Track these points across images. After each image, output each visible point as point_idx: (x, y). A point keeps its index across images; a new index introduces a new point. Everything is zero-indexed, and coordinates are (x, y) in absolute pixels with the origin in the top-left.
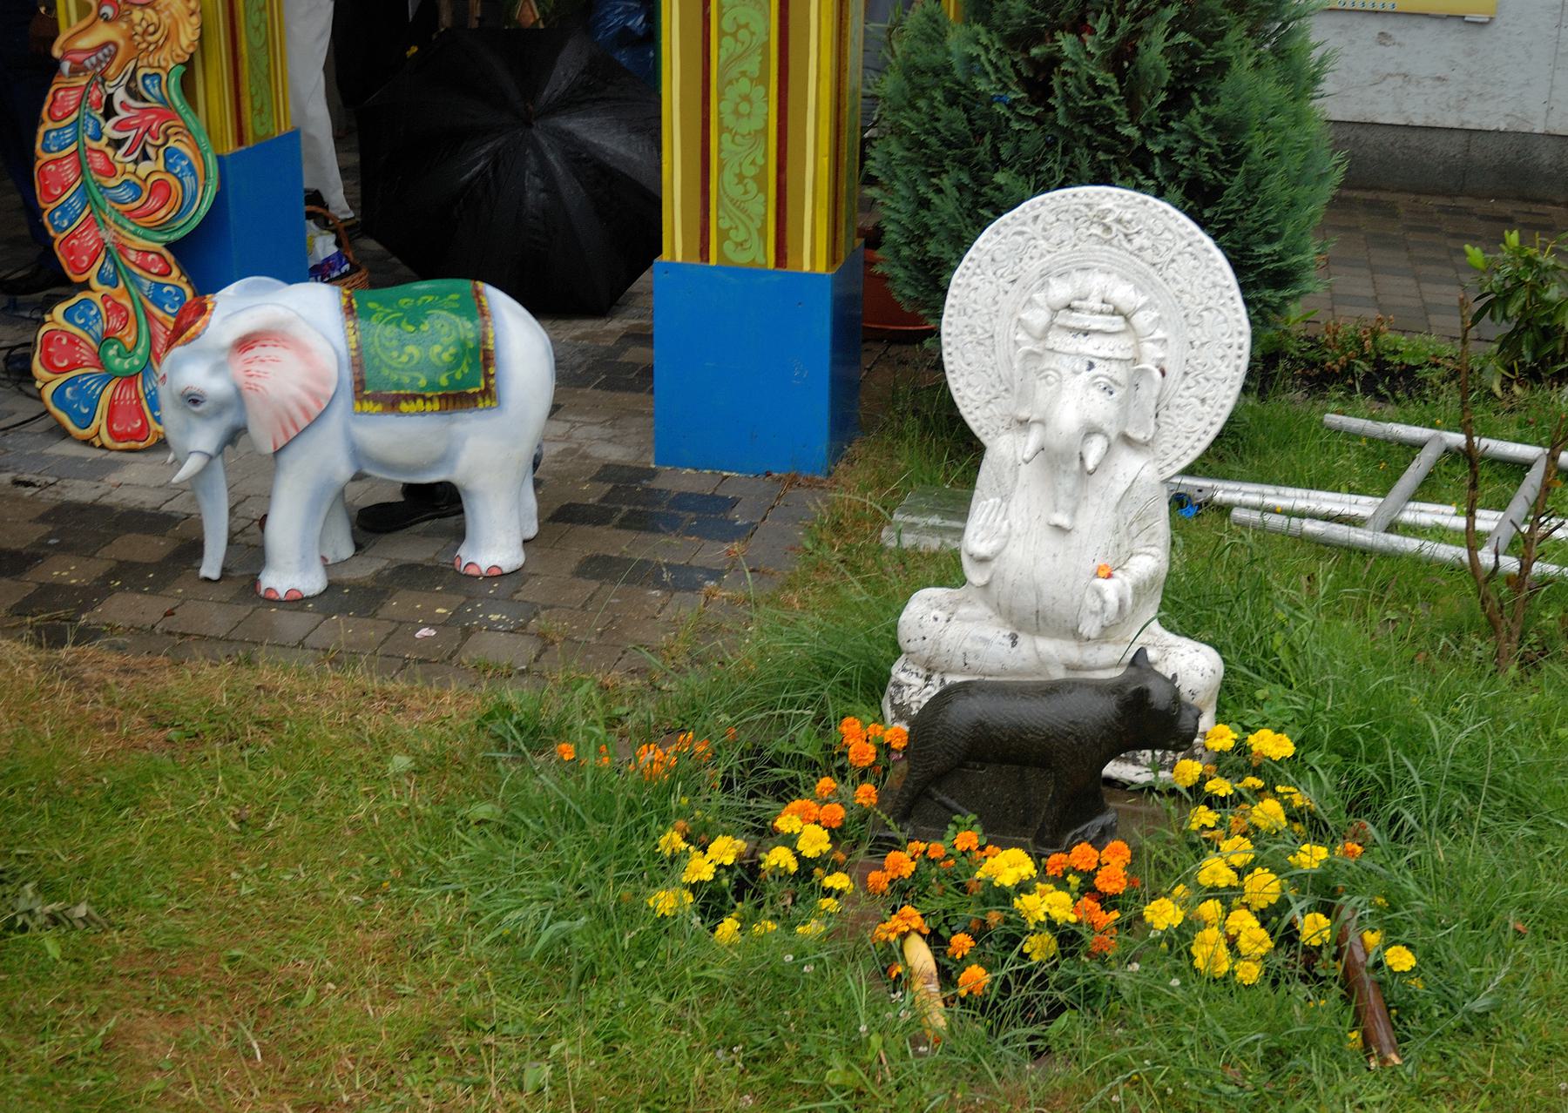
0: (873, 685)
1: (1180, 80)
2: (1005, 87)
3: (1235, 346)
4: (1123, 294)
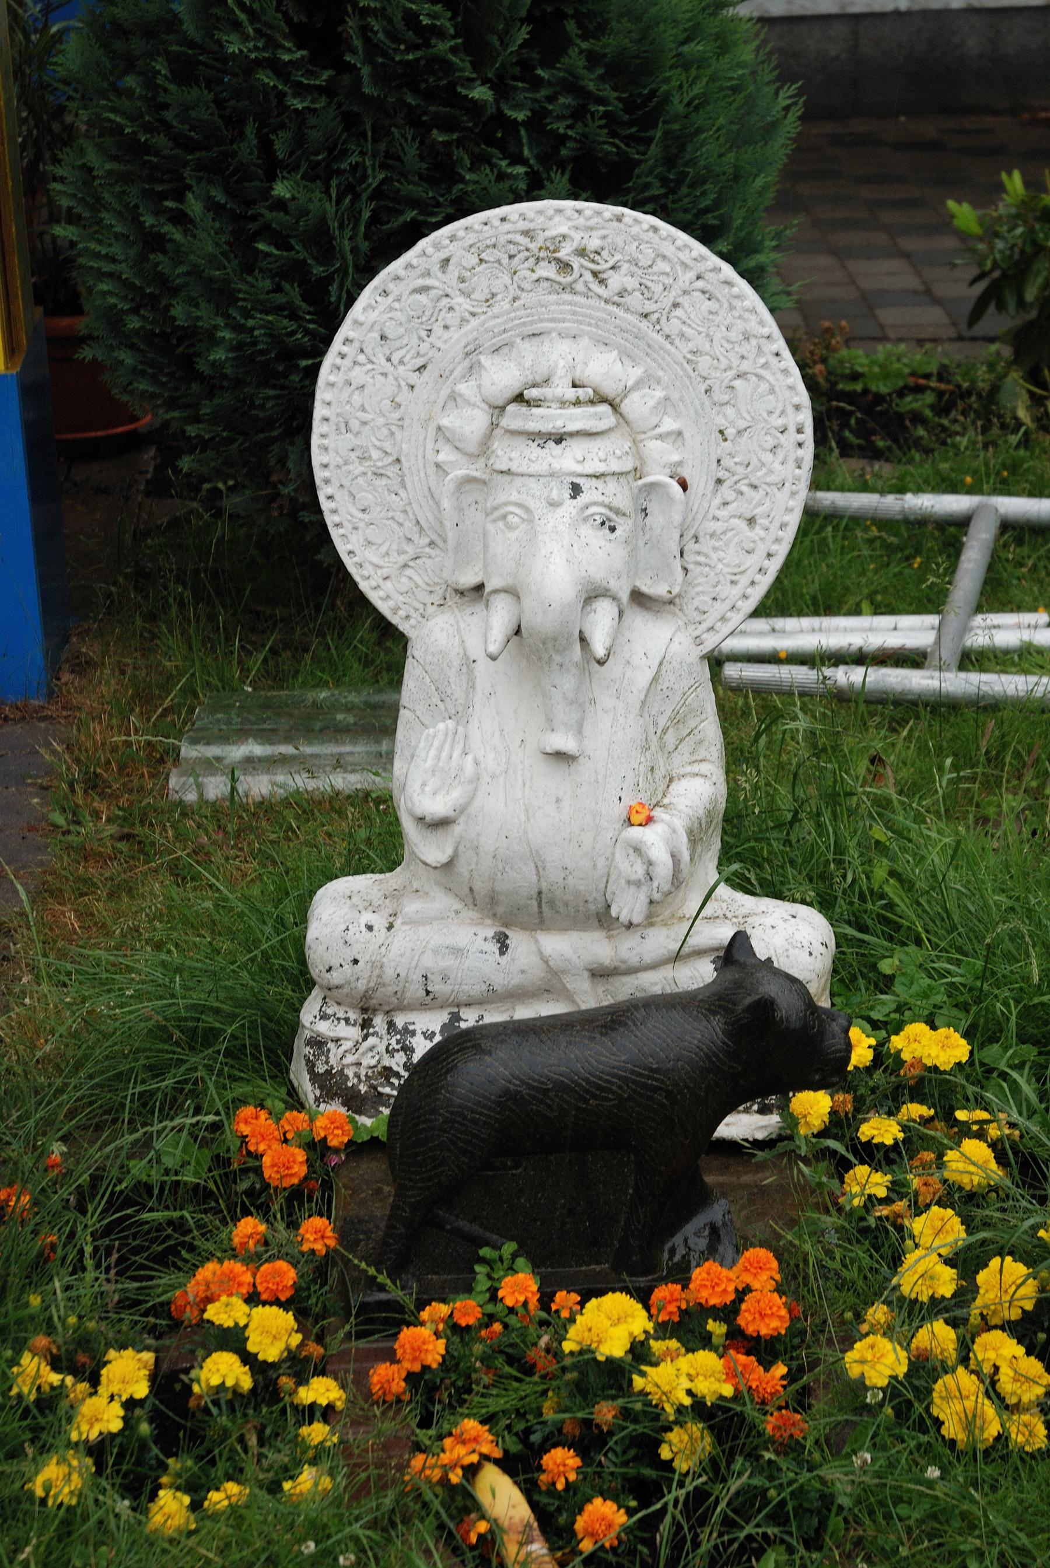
0: (268, 1045)
2: (271, 44)
3: (792, 429)
4: (604, 368)
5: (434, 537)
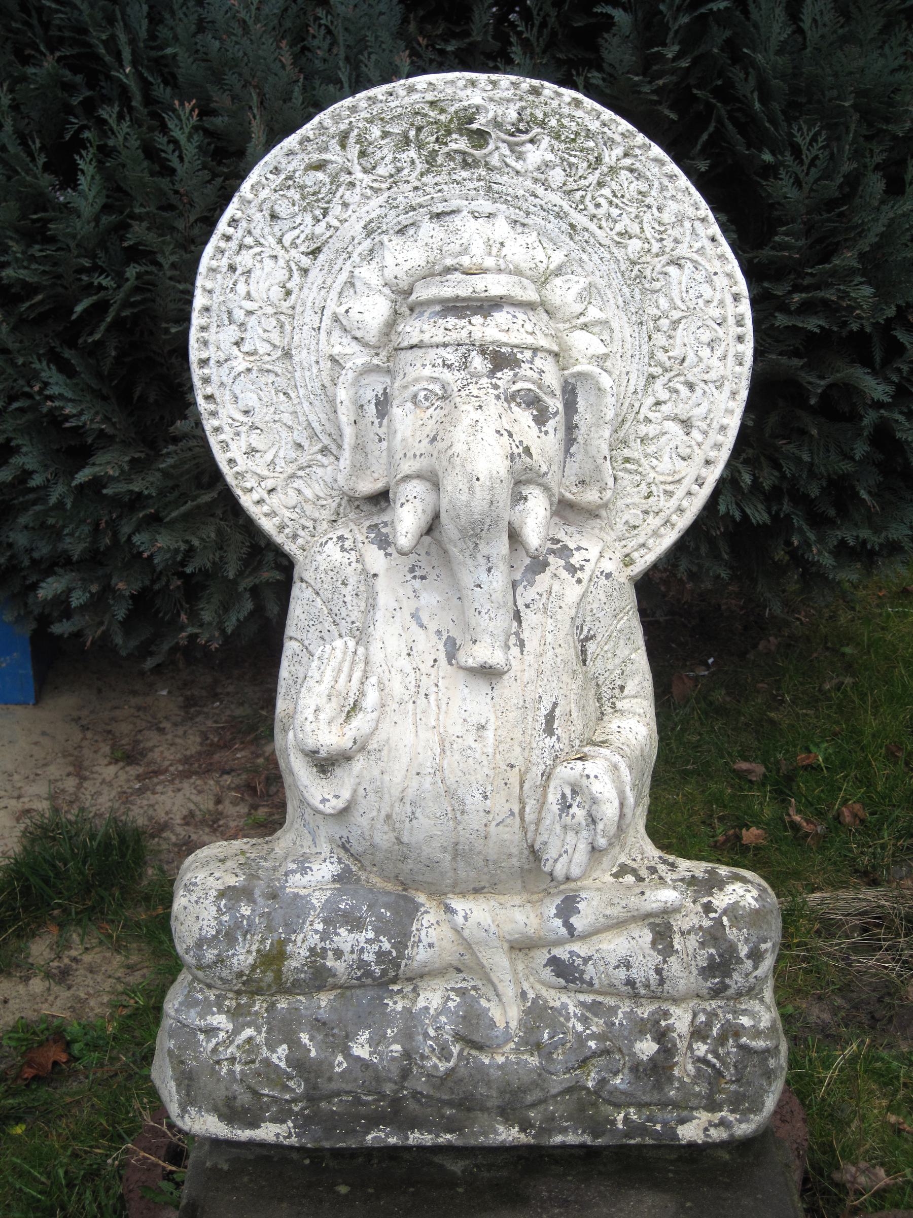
1: (384, 1014)
3: (731, 321)
5: (326, 440)
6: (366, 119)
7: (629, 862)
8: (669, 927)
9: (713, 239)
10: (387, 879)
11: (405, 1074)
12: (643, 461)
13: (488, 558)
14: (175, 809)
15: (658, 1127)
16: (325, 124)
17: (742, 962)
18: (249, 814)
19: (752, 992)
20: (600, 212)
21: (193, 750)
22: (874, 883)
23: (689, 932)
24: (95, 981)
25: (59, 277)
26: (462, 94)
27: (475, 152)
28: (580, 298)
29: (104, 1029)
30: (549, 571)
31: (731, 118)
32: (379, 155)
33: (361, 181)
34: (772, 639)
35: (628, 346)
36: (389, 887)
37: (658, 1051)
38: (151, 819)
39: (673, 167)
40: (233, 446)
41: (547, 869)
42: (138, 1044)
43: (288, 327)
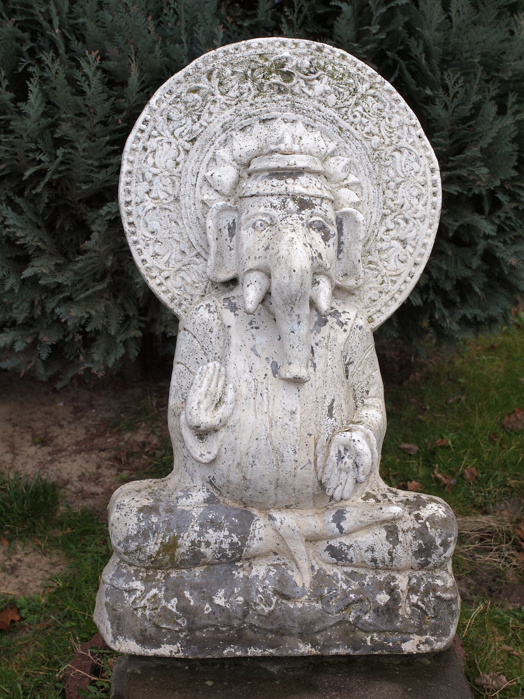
1: (233, 580)
3: (430, 184)
5: (199, 249)
6: (222, 64)
7: (371, 491)
8: (396, 528)
9: (420, 137)
10: (235, 501)
11: (245, 614)
12: (379, 263)
13: (299, 316)
14: (73, 472)
15: (391, 644)
16: (199, 66)
17: (438, 548)
18: (118, 474)
19: (441, 566)
20: (356, 120)
21: (82, 437)
22: (486, 513)
23: (407, 531)
24: (32, 572)
25: (16, 154)
26: (277, 50)
27: (285, 84)
28: (345, 169)
29: (39, 601)
30: (329, 324)
31: (408, 69)
32: (230, 84)
33: (220, 100)
34: (417, 374)
35: (371, 197)
36: (236, 505)
37: (390, 600)
38: (59, 477)
39: (397, 95)
40: (145, 252)
41: (330, 494)
42: (60, 609)
43: (177, 184)
